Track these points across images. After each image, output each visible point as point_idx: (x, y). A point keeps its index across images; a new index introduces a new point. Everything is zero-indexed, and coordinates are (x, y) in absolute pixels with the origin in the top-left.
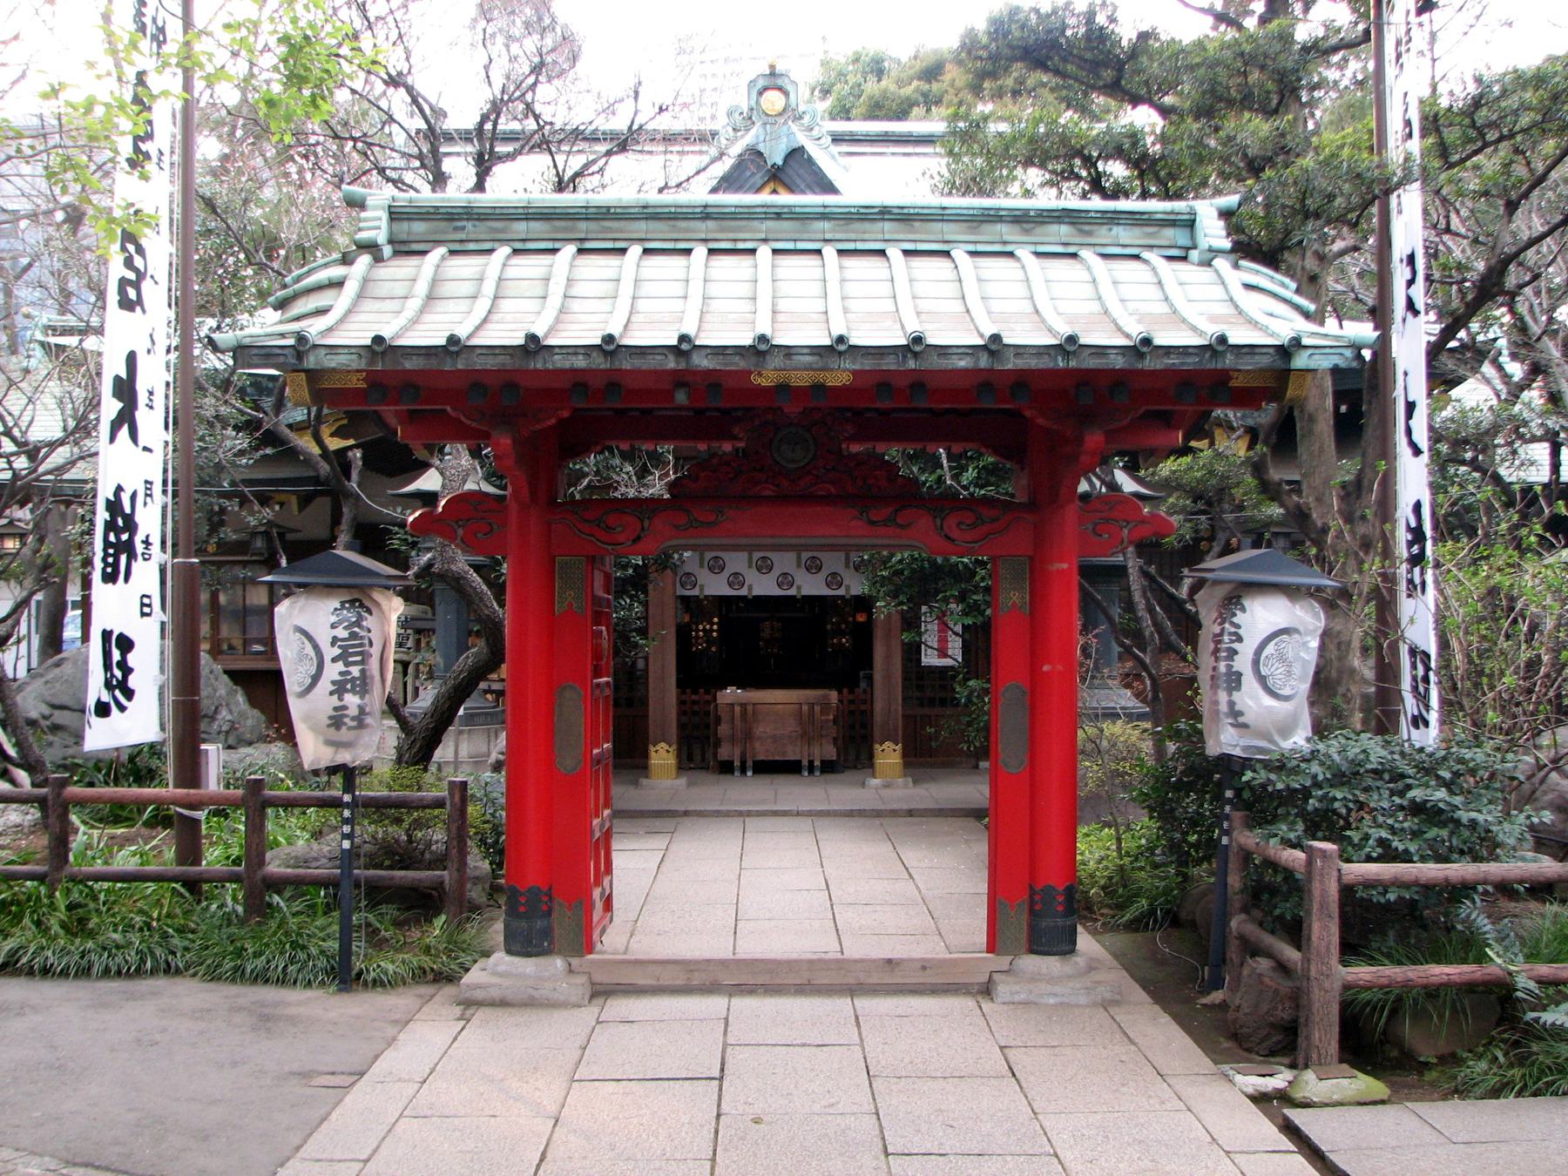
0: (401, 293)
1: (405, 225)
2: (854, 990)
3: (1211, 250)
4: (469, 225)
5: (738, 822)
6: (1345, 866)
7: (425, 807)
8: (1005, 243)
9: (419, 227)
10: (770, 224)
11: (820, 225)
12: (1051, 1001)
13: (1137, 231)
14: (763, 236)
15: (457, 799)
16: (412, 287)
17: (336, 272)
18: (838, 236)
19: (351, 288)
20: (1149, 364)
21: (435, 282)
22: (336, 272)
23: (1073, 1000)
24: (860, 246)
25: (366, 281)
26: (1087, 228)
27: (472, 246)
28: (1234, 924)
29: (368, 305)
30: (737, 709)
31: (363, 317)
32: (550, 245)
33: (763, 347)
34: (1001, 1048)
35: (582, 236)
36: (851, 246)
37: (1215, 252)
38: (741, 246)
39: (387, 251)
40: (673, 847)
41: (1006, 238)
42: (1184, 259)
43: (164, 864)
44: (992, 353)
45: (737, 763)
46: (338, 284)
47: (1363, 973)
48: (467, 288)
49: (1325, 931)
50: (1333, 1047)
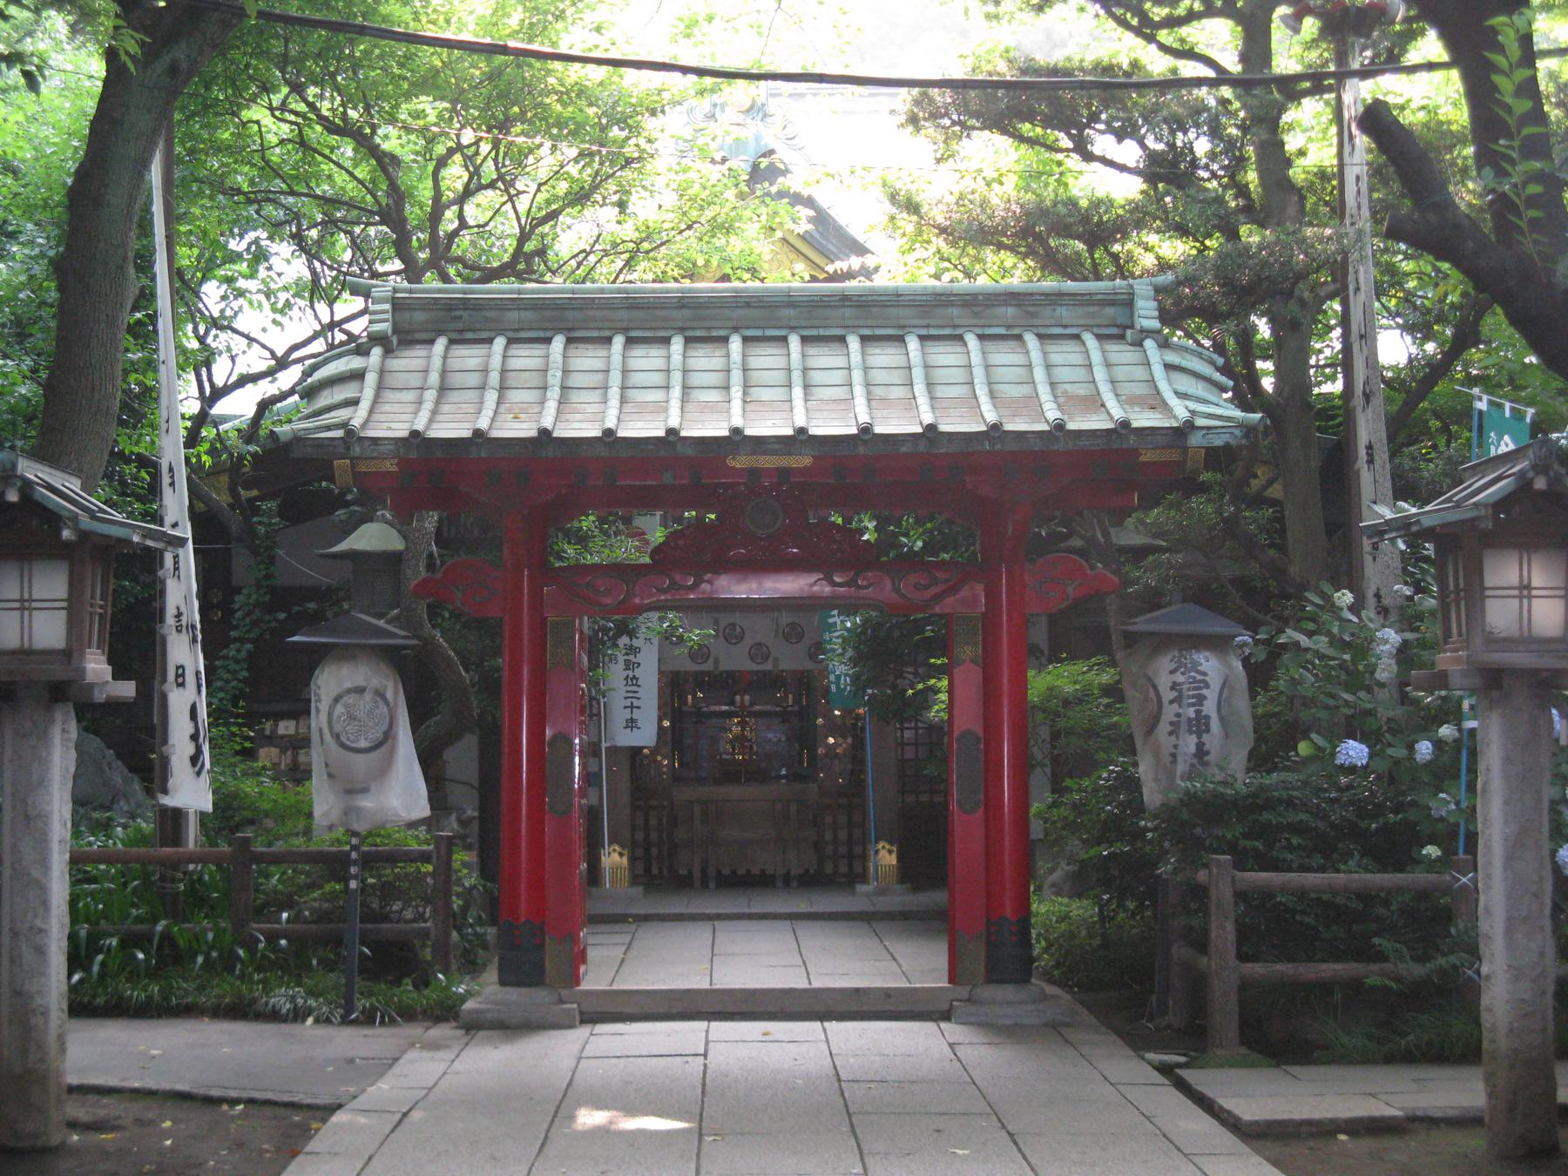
0: (417, 384)
1: (407, 315)
2: (823, 1016)
3: (1142, 331)
4: (465, 314)
5: (708, 926)
6: (1239, 875)
7: (413, 860)
8: (955, 327)
9: (420, 317)
10: (740, 312)
11: (786, 312)
12: (1007, 1022)
13: (1080, 310)
14: (734, 324)
15: (443, 852)
16: (425, 379)
17: (356, 363)
18: (803, 323)
19: (371, 378)
20: (1060, 446)
21: (444, 372)
22: (356, 363)
23: (1026, 1021)
24: (822, 332)
25: (382, 372)
26: (1031, 309)
27: (470, 335)
28: (1174, 950)
29: (389, 395)
30: (697, 809)
31: (387, 408)
32: (541, 334)
33: (737, 438)
34: (951, 1045)
35: (570, 325)
36: (814, 332)
37: (1148, 333)
38: (715, 333)
39: (395, 340)
40: (636, 944)
41: (958, 321)
42: (1122, 337)
43: (1519, 195)
44: (929, 440)
45: (697, 875)
46: (358, 376)
47: (1256, 969)
48: (473, 379)
49: (1223, 933)
50: (1233, 1034)
